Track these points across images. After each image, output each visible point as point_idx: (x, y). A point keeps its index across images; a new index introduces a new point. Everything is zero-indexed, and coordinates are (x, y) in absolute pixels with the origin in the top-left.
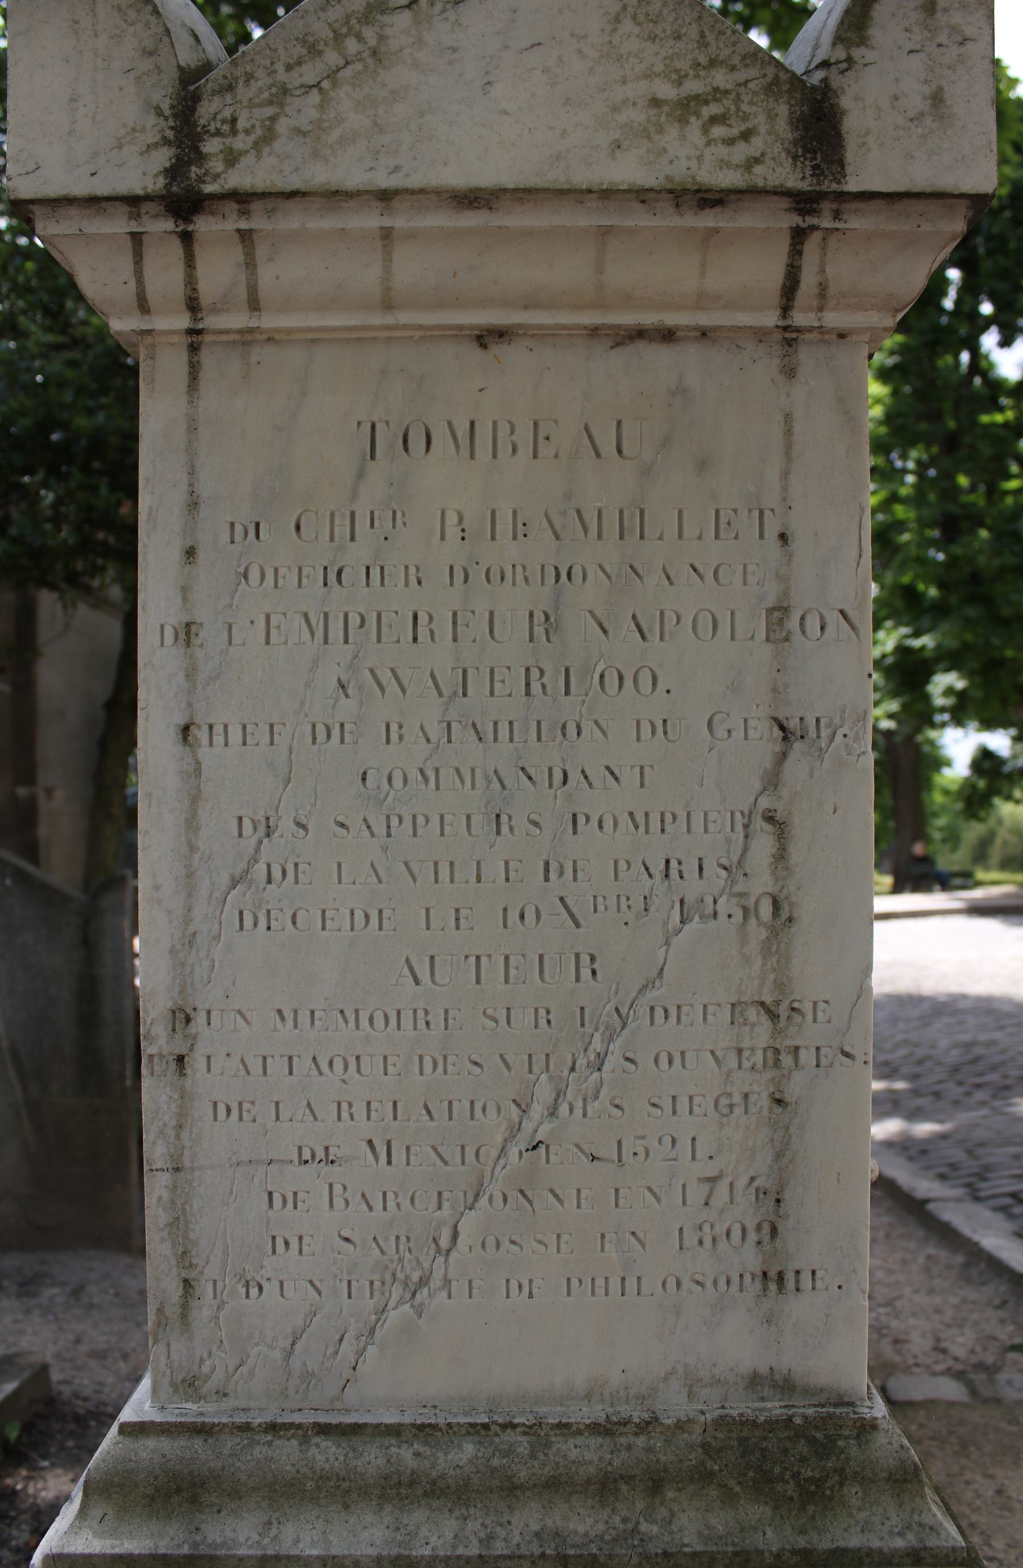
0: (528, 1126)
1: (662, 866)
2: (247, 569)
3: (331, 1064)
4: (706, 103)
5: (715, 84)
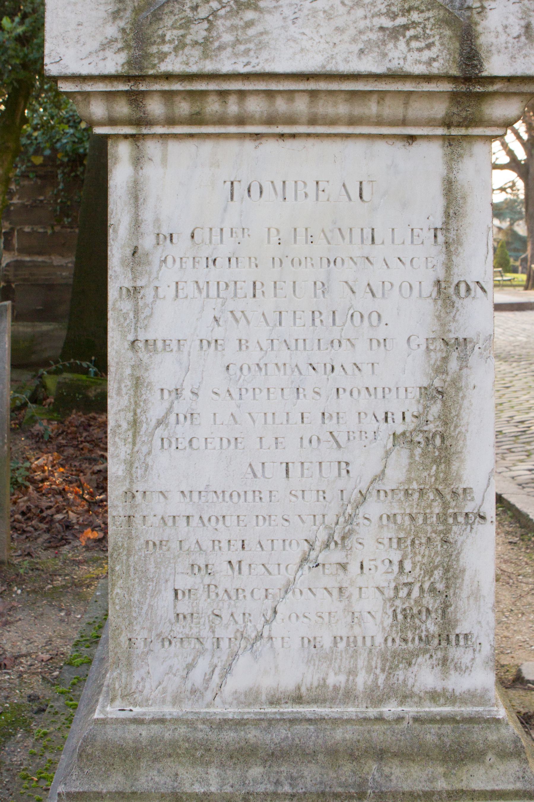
0: (313, 554)
1: (383, 416)
2: (166, 258)
3: (209, 520)
4: (408, 29)
5: (413, 20)
